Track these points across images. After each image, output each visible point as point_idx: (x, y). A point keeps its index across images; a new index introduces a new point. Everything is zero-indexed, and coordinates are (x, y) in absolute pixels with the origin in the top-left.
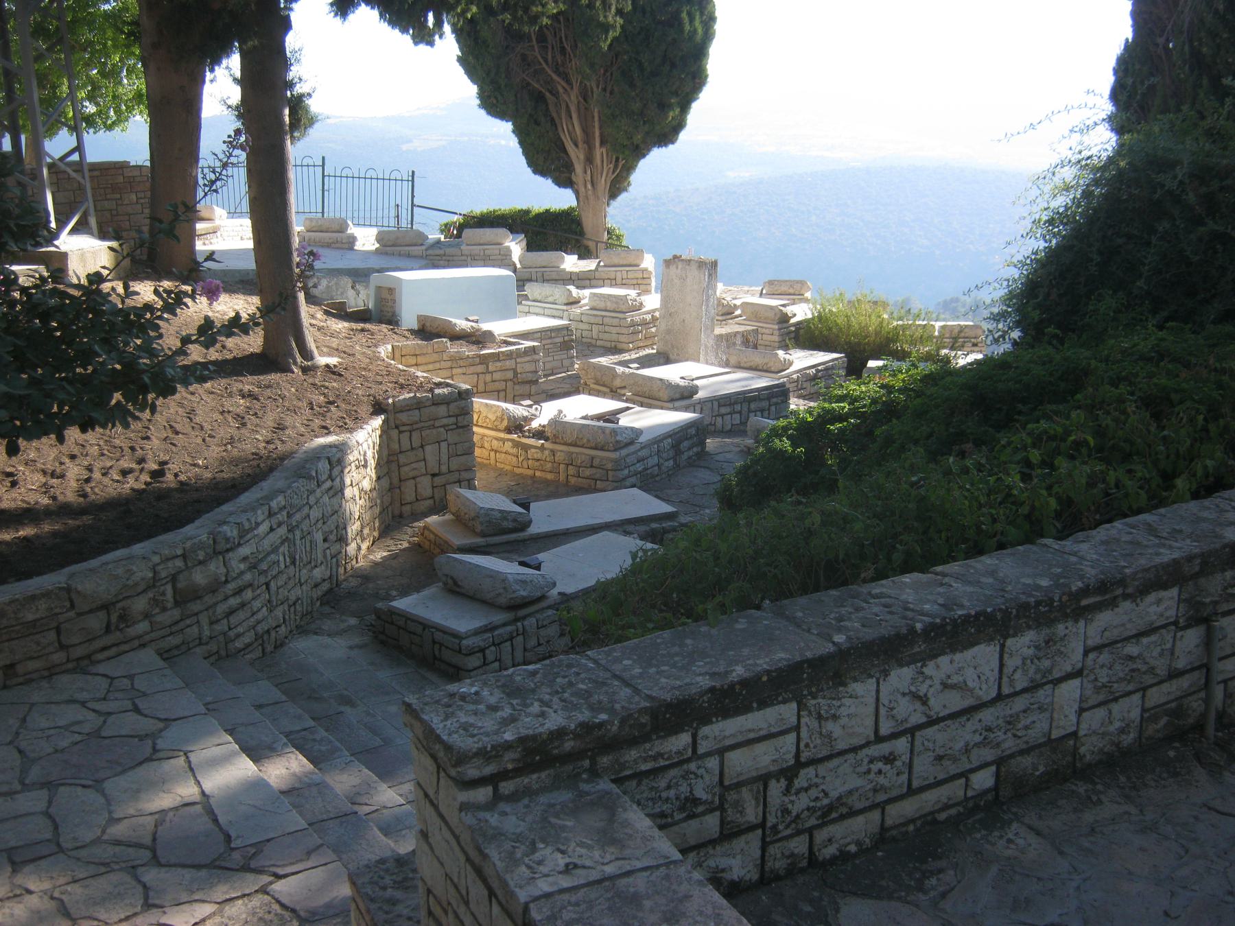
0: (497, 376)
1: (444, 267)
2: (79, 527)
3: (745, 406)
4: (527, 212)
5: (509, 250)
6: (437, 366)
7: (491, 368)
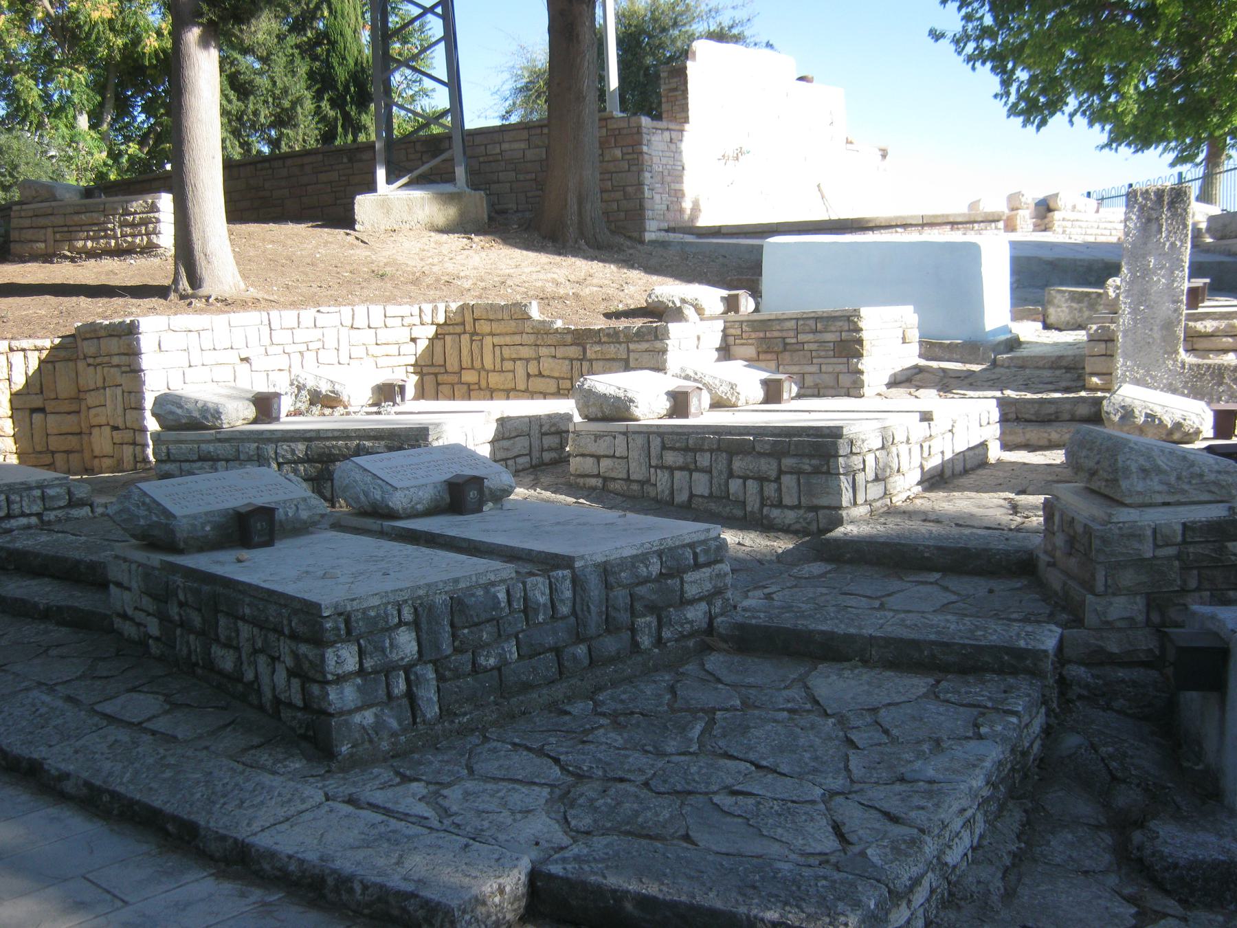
1: (228, 193)
2: (1224, 862)
3: (721, 464)
7: (589, 354)
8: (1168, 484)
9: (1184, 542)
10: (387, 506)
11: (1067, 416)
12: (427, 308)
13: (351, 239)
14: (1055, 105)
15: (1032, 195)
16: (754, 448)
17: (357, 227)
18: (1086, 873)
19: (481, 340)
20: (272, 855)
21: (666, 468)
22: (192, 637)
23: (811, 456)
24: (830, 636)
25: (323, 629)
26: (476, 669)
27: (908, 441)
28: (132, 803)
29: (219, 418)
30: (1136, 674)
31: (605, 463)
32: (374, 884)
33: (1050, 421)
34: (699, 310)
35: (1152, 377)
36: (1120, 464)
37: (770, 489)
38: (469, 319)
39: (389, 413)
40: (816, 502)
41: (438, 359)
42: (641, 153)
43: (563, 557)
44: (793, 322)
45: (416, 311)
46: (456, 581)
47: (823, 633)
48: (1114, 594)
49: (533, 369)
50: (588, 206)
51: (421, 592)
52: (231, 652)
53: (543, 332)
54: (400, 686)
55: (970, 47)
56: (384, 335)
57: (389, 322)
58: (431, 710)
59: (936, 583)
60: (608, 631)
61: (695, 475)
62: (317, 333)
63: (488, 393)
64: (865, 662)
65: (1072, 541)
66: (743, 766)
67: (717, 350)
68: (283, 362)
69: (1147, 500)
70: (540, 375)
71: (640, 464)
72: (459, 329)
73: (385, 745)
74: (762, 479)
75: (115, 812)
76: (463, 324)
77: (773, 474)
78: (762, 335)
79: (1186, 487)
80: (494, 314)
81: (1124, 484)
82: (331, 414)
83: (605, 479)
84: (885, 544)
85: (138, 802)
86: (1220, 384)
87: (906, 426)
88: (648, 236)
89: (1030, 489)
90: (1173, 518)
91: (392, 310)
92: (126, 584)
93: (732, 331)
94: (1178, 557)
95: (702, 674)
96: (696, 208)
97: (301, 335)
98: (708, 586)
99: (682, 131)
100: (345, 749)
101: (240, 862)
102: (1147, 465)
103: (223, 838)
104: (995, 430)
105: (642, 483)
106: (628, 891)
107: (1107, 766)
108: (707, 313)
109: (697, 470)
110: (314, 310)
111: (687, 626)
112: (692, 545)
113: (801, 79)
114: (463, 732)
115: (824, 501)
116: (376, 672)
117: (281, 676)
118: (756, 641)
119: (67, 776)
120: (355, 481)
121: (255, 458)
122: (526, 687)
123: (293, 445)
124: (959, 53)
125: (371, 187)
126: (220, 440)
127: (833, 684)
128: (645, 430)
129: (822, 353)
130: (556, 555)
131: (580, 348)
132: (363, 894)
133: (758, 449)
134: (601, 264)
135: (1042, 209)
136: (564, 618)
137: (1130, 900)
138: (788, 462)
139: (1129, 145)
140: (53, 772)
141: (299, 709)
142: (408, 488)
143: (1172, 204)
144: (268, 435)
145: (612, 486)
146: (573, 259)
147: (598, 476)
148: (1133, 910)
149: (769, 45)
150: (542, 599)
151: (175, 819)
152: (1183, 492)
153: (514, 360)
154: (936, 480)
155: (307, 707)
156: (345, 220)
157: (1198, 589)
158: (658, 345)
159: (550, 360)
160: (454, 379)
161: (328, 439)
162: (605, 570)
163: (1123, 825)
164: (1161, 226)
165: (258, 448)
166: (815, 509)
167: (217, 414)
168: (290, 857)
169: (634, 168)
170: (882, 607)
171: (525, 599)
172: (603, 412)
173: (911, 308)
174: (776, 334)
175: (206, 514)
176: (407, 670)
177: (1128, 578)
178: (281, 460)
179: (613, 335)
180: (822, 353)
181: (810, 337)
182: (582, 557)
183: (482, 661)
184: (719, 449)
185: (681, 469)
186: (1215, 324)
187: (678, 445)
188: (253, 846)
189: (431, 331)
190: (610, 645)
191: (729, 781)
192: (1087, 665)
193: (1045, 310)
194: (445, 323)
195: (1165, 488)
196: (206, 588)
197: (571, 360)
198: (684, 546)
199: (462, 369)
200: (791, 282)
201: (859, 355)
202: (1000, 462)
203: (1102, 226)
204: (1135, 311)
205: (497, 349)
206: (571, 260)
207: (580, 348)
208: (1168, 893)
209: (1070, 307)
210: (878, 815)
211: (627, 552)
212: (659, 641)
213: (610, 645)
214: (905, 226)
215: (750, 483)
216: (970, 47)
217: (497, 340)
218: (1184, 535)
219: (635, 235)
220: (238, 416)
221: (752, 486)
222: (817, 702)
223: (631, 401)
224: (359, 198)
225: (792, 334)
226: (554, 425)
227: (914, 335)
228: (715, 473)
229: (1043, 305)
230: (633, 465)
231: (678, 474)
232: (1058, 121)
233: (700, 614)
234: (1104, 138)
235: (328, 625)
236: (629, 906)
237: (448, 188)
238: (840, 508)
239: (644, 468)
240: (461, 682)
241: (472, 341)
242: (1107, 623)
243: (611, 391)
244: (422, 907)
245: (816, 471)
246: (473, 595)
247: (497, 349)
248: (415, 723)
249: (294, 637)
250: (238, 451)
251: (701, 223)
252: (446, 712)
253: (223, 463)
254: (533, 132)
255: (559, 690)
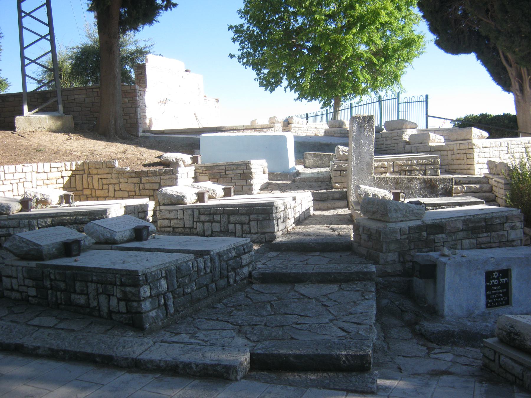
0: (147, 186)
3: (225, 219)
4: (491, 115)
5: (411, 136)
6: (110, 176)
7: (143, 181)
8: (403, 214)
9: (409, 233)
10: (114, 239)
11: (331, 198)
12: (68, 164)
13: (16, 135)
14: (278, 83)
15: (281, 118)
16: (238, 212)
17: (16, 130)
18: (406, 340)
19: (92, 177)
20: (152, 361)
21: (201, 222)
22: (59, 293)
23: (262, 214)
24: (298, 274)
25: (139, 280)
26: (184, 294)
27: (290, 208)
28: (76, 353)
29: (10, 210)
30: (397, 279)
31: (173, 222)
32: (200, 364)
33: (325, 200)
34: (184, 162)
35: (364, 183)
36: (388, 208)
37: (246, 227)
38: (86, 168)
39: (74, 206)
40: (264, 231)
41: (73, 185)
42: (136, 100)
43: (205, 251)
44: (224, 167)
45: (63, 165)
46: (177, 260)
47: (294, 273)
48: (389, 252)
49: (117, 187)
50: (119, 122)
51: (167, 265)
52: (83, 296)
53: (121, 173)
54: (162, 302)
55: (245, 60)
56: (50, 175)
57: (53, 170)
58: (172, 310)
59: (319, 255)
60: (221, 278)
61: (214, 224)
62: (23, 175)
63: (96, 199)
64: (312, 282)
65: (370, 236)
66: (295, 316)
67: (193, 178)
68: (10, 187)
69: (397, 220)
70: (120, 190)
71: (190, 221)
72: (82, 172)
73: (160, 324)
74: (242, 224)
75: (67, 358)
76: (84, 170)
77: (247, 221)
78: (211, 172)
79: (408, 215)
80: (98, 166)
81: (390, 215)
82: (46, 208)
83: (174, 228)
84: (297, 243)
85: (79, 352)
86: (387, 184)
87: (290, 202)
88: (140, 134)
89: (333, 223)
90: (405, 225)
91: (53, 165)
92: (14, 275)
93: (198, 171)
94: (407, 238)
95: (254, 291)
96: (151, 123)
97: (17, 176)
98: (248, 260)
99: (145, 91)
100: (147, 326)
101: (137, 366)
102: (396, 208)
103: (127, 359)
104: (311, 204)
105: (190, 228)
106: (290, 354)
107: (399, 308)
108: (186, 164)
109: (214, 222)
110: (21, 165)
111: (243, 275)
112: (242, 245)
113: (186, 71)
114: (184, 317)
115: (268, 230)
116: (155, 296)
117: (114, 302)
118: (267, 278)
119: (39, 348)
120: (97, 230)
121: (28, 226)
122: (199, 300)
123: (45, 220)
124: (240, 62)
125: (21, 113)
126: (10, 219)
127: (304, 289)
128: (191, 207)
129: (236, 178)
130: (202, 251)
131: (139, 179)
132: (196, 368)
133: (240, 212)
134: (128, 145)
135: (286, 123)
136: (209, 273)
137: (423, 345)
138: (253, 217)
139: (306, 98)
140: (30, 347)
141: (124, 313)
142: (121, 232)
143: (368, 121)
144: (33, 216)
145: (177, 230)
146: (116, 144)
147: (170, 227)
148: (426, 348)
149: (160, 55)
150: (203, 267)
151: (100, 356)
152: (407, 217)
153: (108, 184)
154: (299, 222)
155: (128, 312)
156: (11, 127)
157: (414, 249)
158: (174, 176)
159: (125, 184)
160: (81, 193)
161: (61, 216)
162: (219, 255)
163: (411, 325)
164: (365, 129)
165: (29, 222)
166: (264, 233)
167: (8, 208)
168: (160, 361)
169: (133, 106)
170: (307, 264)
171: (197, 266)
172: (171, 201)
173: (264, 161)
174: (217, 171)
175: (53, 244)
176: (164, 295)
177: (393, 247)
178: (40, 226)
179: (154, 173)
180: (236, 178)
181: (231, 172)
182: (213, 251)
183: (186, 290)
184: (224, 213)
185: (208, 222)
186: (378, 163)
187: (206, 213)
188: (142, 359)
189: (70, 173)
190: (222, 283)
191: (294, 321)
192: (381, 277)
193: (304, 161)
194: (76, 170)
195: (402, 216)
196: (68, 272)
197: (135, 184)
198: (240, 246)
199: (83, 189)
200: (211, 151)
201: (251, 179)
202: (314, 215)
203: (309, 129)
204: (357, 159)
205: (100, 180)
206: (115, 144)
207: (139, 179)
208: (432, 342)
209: (313, 160)
210: (352, 324)
211: (225, 248)
212: (235, 281)
213: (222, 283)
214: (237, 130)
215: (237, 225)
216: (245, 60)
217: (100, 176)
218: (409, 231)
219: (135, 133)
220: (16, 208)
221: (238, 227)
222: (304, 296)
223: (184, 197)
224: (17, 118)
225: (223, 171)
226: (143, 208)
227: (267, 170)
228: (222, 222)
229: (303, 159)
230: (186, 222)
231: (206, 224)
232: (279, 90)
233: (247, 270)
234: (296, 95)
235: (141, 278)
236: (291, 359)
237: (56, 114)
238: (274, 232)
239: (191, 223)
240: (180, 299)
241: (88, 177)
242: (387, 262)
243: (174, 193)
244: (223, 368)
245: (264, 219)
246: (183, 266)
247: (100, 180)
248: (167, 315)
249: (122, 284)
250: (19, 223)
251: (153, 128)
252: (176, 311)
253: (12, 229)
254: (88, 91)
255: (209, 301)
